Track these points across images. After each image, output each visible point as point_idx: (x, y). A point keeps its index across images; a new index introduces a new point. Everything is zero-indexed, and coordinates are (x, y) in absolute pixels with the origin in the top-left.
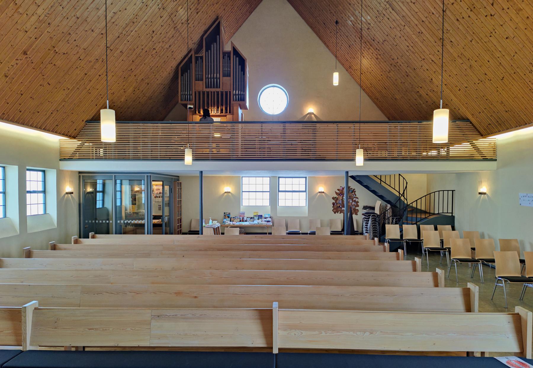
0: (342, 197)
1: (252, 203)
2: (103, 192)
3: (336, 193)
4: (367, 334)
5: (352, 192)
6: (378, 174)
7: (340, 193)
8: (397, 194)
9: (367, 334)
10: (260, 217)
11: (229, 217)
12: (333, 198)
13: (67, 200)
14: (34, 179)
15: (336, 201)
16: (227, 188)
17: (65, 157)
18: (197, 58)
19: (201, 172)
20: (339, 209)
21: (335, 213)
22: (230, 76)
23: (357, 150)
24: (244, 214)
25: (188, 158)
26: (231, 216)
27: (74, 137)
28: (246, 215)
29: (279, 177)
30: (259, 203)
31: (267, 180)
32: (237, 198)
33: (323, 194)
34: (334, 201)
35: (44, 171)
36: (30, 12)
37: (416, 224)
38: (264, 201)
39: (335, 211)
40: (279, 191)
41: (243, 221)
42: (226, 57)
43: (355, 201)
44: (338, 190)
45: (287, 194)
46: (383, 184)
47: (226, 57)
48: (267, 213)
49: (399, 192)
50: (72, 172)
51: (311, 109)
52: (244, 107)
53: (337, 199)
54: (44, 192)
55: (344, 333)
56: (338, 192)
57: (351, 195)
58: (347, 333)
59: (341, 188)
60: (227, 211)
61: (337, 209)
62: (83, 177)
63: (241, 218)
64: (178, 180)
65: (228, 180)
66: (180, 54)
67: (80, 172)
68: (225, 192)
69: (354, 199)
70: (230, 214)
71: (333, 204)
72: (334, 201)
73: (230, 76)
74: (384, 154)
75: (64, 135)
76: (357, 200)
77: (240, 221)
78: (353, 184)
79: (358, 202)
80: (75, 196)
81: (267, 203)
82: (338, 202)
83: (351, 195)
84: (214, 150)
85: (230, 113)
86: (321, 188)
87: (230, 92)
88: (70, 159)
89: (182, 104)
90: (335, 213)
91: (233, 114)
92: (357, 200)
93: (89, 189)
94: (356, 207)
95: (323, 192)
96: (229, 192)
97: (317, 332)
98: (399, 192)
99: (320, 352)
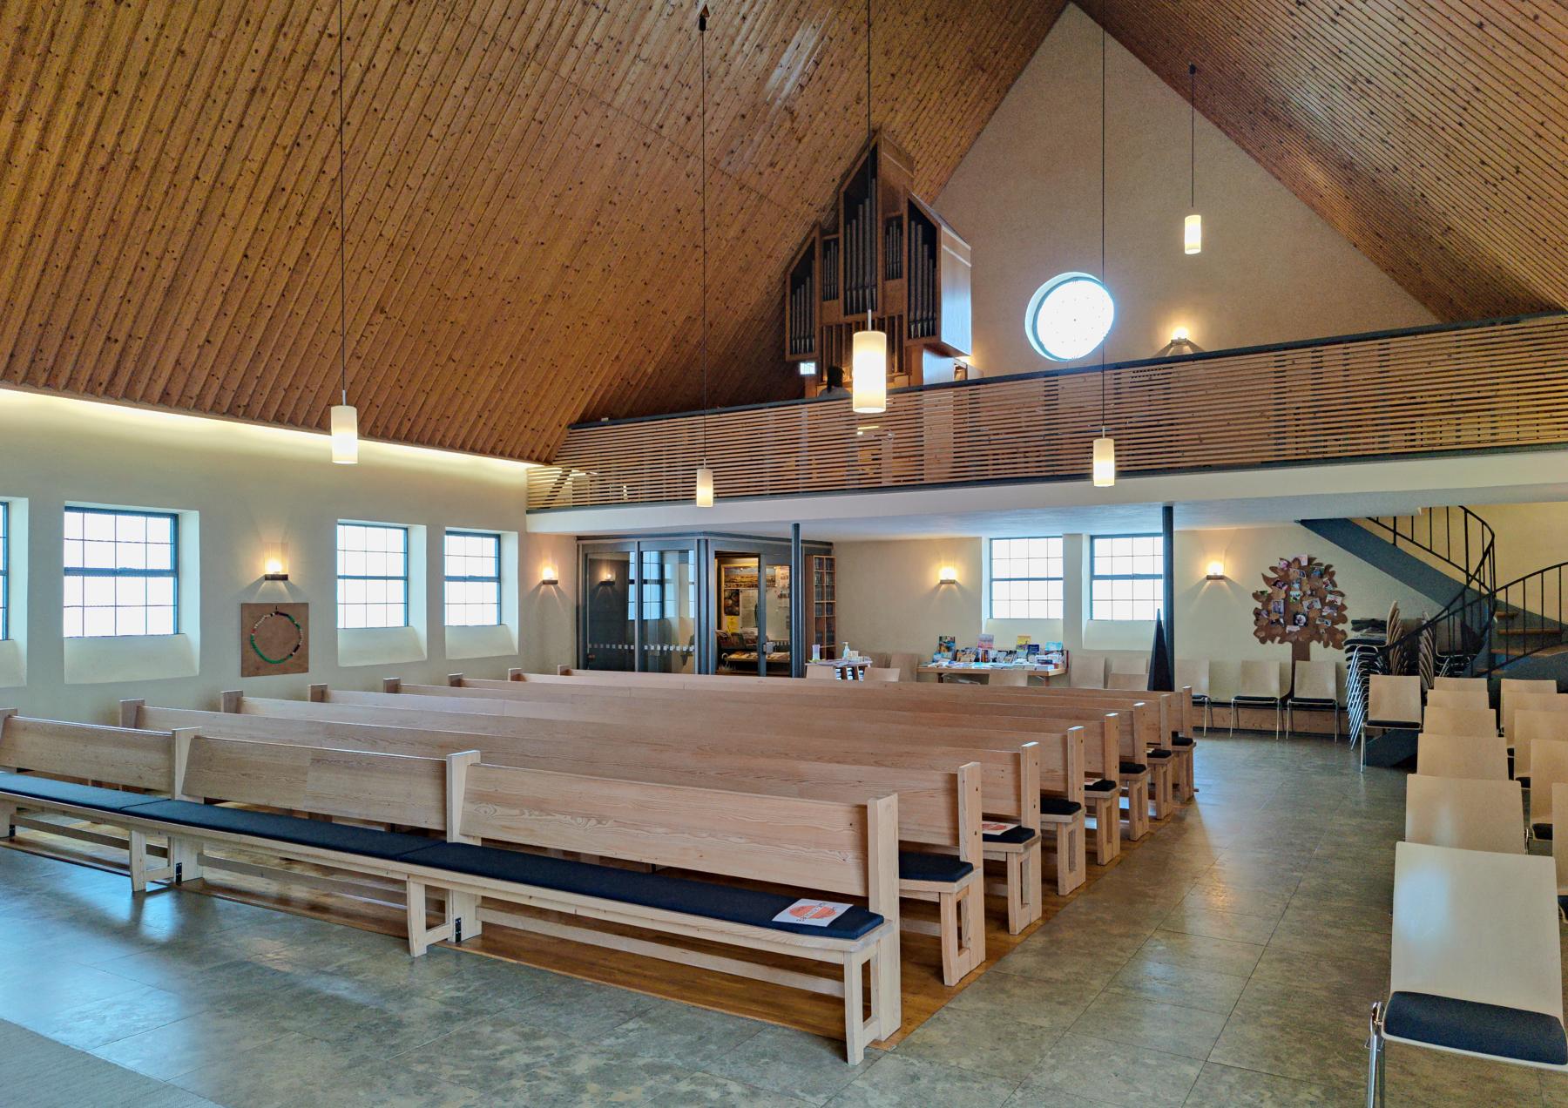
0: (1287, 592)
1: (1019, 612)
2: (661, 582)
3: (1266, 579)
4: (593, 822)
5: (1321, 576)
6: (1384, 510)
7: (1280, 579)
8: (1461, 578)
9: (593, 822)
10: (1034, 649)
11: (949, 649)
12: (1256, 596)
13: (546, 598)
14: (468, 553)
15: (1265, 604)
16: (947, 571)
17: (546, 505)
18: (826, 245)
19: (797, 526)
20: (1279, 629)
21: (1263, 641)
22: (900, 276)
23: (1096, 442)
24: (991, 641)
25: (705, 492)
26: (959, 646)
27: (548, 462)
28: (997, 645)
29: (1092, 538)
30: (1038, 612)
31: (1057, 546)
32: (968, 598)
33: (1223, 583)
34: (1259, 606)
35: (498, 537)
36: (369, 236)
37: (1488, 674)
38: (1047, 605)
39: (1263, 634)
40: (1093, 577)
41: (986, 660)
42: (893, 230)
43: (1332, 604)
44: (1273, 569)
45: (1062, 580)
46: (1402, 544)
47: (893, 230)
48: (1051, 642)
49: (1467, 572)
50: (560, 537)
51: (1182, 330)
52: (943, 351)
53: (1270, 598)
54: (498, 579)
55: (558, 816)
56: (1273, 575)
57: (1319, 583)
58: (562, 817)
59: (1283, 564)
60: (948, 634)
61: (1267, 630)
62: (587, 550)
63: (981, 651)
64: (828, 552)
65: (954, 548)
66: (787, 242)
67: (579, 538)
68: (942, 582)
69: (1329, 598)
70: (953, 640)
71: (1257, 613)
72: (1259, 606)
73: (900, 276)
74: (1397, 441)
75: (529, 459)
76: (1339, 600)
77: (977, 660)
78: (1326, 552)
79: (1343, 607)
80: (567, 587)
81: (1057, 612)
82: (1271, 607)
83: (1319, 583)
84: (867, 469)
85: (900, 370)
86: (1216, 565)
87: (901, 317)
88: (546, 509)
89: (958, 353)
90: (1263, 641)
91: (909, 373)
92: (1339, 600)
93: (606, 575)
94: (1335, 622)
95: (1221, 578)
96: (953, 582)
97: (517, 812)
98: (1467, 572)
99: (499, 847)
